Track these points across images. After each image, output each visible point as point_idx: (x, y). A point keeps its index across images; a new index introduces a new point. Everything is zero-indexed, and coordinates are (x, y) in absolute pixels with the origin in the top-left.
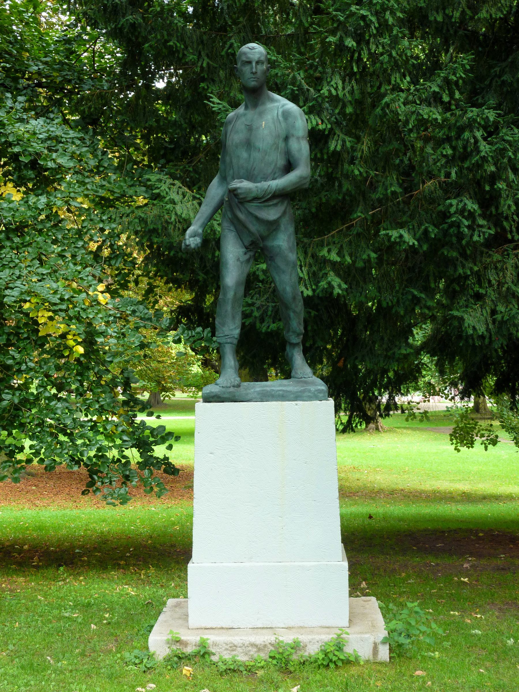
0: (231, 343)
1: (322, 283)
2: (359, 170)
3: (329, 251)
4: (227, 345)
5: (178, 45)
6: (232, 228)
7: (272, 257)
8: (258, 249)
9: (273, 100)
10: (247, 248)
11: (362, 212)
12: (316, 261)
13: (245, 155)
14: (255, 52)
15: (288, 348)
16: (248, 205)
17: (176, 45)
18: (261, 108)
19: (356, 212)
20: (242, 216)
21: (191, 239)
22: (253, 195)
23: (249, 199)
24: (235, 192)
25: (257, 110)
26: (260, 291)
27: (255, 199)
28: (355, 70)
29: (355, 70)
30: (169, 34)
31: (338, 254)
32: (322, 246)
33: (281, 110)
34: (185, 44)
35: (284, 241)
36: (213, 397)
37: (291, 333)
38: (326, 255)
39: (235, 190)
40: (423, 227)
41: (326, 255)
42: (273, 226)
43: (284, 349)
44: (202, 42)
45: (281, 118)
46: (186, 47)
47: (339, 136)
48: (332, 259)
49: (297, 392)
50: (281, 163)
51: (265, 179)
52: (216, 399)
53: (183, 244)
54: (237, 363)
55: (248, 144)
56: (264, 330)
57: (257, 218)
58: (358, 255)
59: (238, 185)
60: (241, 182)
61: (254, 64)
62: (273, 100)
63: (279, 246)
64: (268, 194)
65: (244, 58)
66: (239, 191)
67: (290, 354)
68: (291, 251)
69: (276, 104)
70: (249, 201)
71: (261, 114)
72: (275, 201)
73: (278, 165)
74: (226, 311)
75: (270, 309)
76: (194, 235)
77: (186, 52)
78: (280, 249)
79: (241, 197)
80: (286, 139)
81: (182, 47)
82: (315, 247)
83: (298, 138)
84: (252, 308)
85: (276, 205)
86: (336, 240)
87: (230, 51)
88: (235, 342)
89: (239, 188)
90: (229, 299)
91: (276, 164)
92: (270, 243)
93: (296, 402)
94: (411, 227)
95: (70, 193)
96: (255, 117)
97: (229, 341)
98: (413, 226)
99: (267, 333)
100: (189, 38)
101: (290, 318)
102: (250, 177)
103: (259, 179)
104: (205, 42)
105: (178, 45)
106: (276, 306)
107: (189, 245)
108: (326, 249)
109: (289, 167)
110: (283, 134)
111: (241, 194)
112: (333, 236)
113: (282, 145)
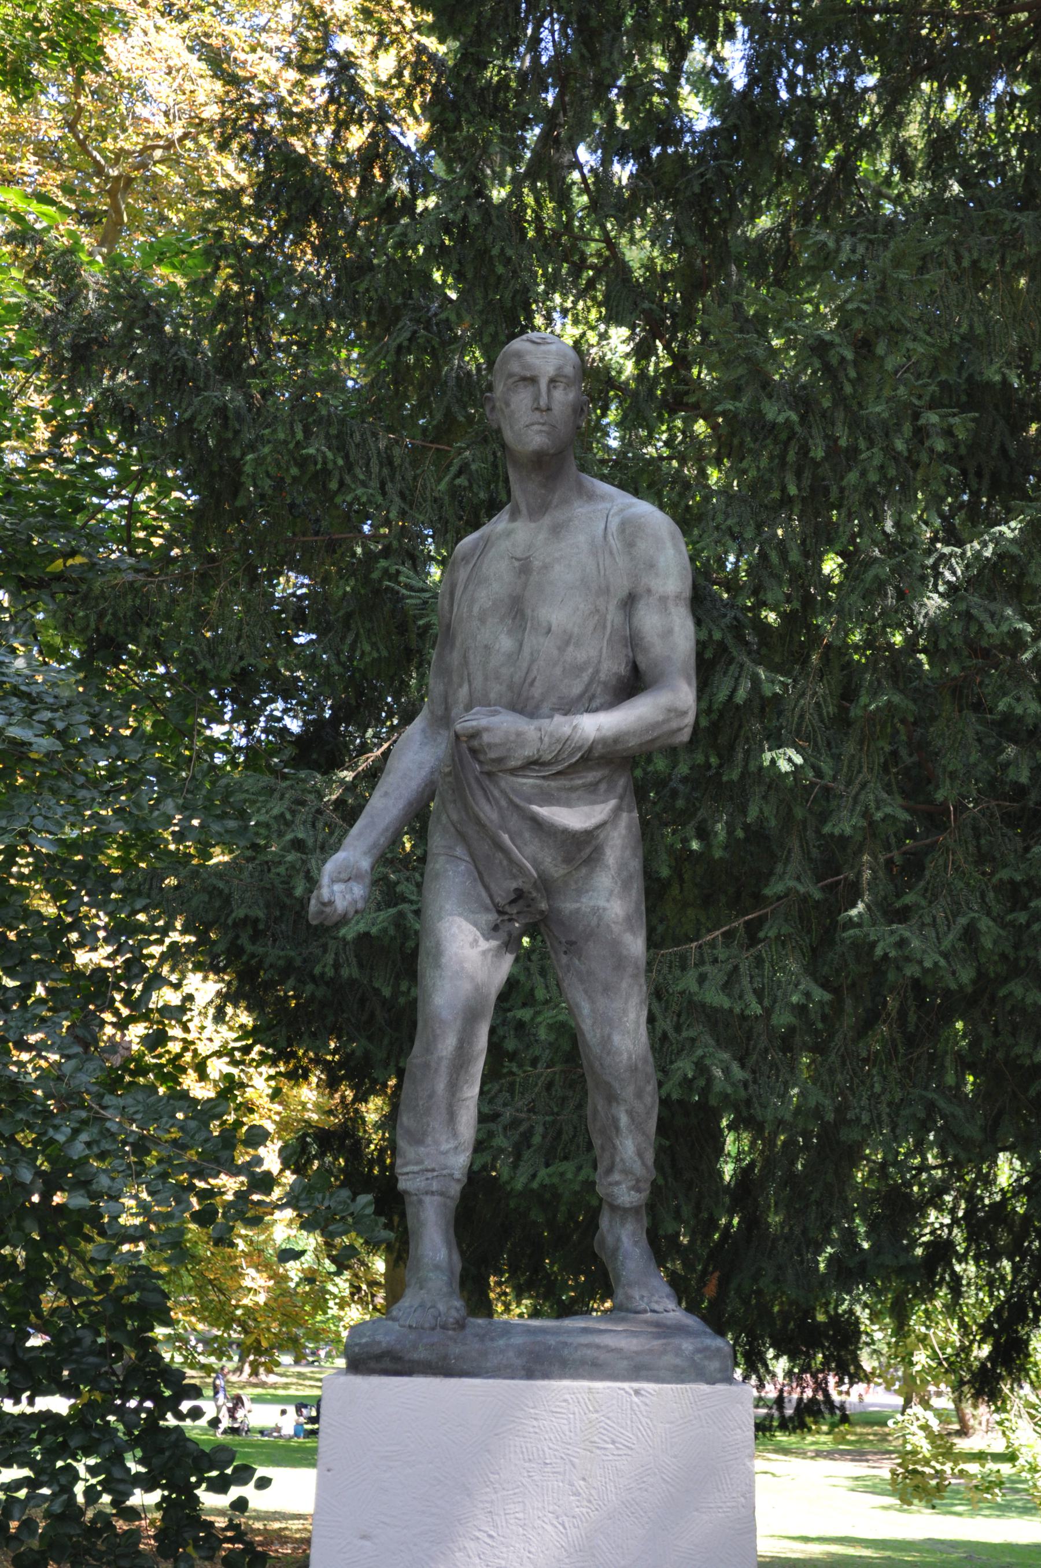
0: (442, 1194)
1: (679, 1064)
2: (790, 760)
3: (702, 979)
4: (427, 1199)
5: (330, 455)
6: (460, 851)
7: (571, 943)
8: (535, 923)
9: (591, 496)
10: (501, 913)
11: (798, 879)
12: (666, 1009)
13: (506, 643)
14: (549, 352)
15: (604, 1222)
16: (508, 782)
17: (325, 457)
18: (558, 515)
19: (781, 878)
20: (489, 813)
21: (337, 887)
22: (529, 752)
23: (513, 764)
24: (475, 743)
25: (547, 520)
26: (512, 1084)
27: (533, 764)
28: (793, 490)
29: (793, 490)
30: (307, 432)
31: (727, 987)
32: (684, 968)
33: (614, 524)
34: (346, 457)
35: (610, 901)
36: (379, 1357)
37: (616, 1177)
38: (694, 987)
39: (475, 735)
40: (963, 921)
41: (694, 987)
42: (581, 848)
43: (592, 1224)
44: (390, 463)
45: (615, 543)
46: (349, 467)
47: (742, 666)
48: (708, 1000)
49: (637, 1353)
50: (613, 667)
51: (570, 707)
52: (386, 1363)
53: (313, 902)
54: (456, 1257)
55: (517, 611)
56: (519, 1185)
57: (538, 824)
58: (779, 993)
59: (484, 722)
60: (495, 713)
61: (543, 384)
62: (591, 496)
63: (595, 910)
64: (571, 755)
65: (515, 367)
66: (486, 738)
67: (610, 1240)
68: (631, 929)
69: (601, 506)
70: (514, 771)
71: (557, 531)
72: (591, 776)
73: (603, 676)
74: (431, 1097)
75: (539, 1129)
76: (349, 877)
77: (348, 479)
78: (600, 918)
79: (493, 755)
80: (630, 602)
81: (340, 462)
82: (665, 970)
83: (663, 599)
84: (492, 1126)
85: (592, 788)
86: (721, 953)
87: (458, 481)
88: (455, 1190)
89: (487, 729)
90: (440, 1059)
91: (597, 671)
92: (568, 906)
93: (636, 1385)
94: (928, 920)
95: (32, 818)
96: (541, 537)
97: (435, 1186)
98: (934, 918)
99: (527, 1193)
100: (357, 446)
101: (617, 1129)
102: (522, 704)
103: (545, 709)
104: (397, 462)
105: (330, 455)
106: (554, 1122)
107: (331, 903)
108: (692, 975)
109: (633, 683)
110: (621, 586)
111: (490, 746)
112: (713, 944)
113: (613, 616)
